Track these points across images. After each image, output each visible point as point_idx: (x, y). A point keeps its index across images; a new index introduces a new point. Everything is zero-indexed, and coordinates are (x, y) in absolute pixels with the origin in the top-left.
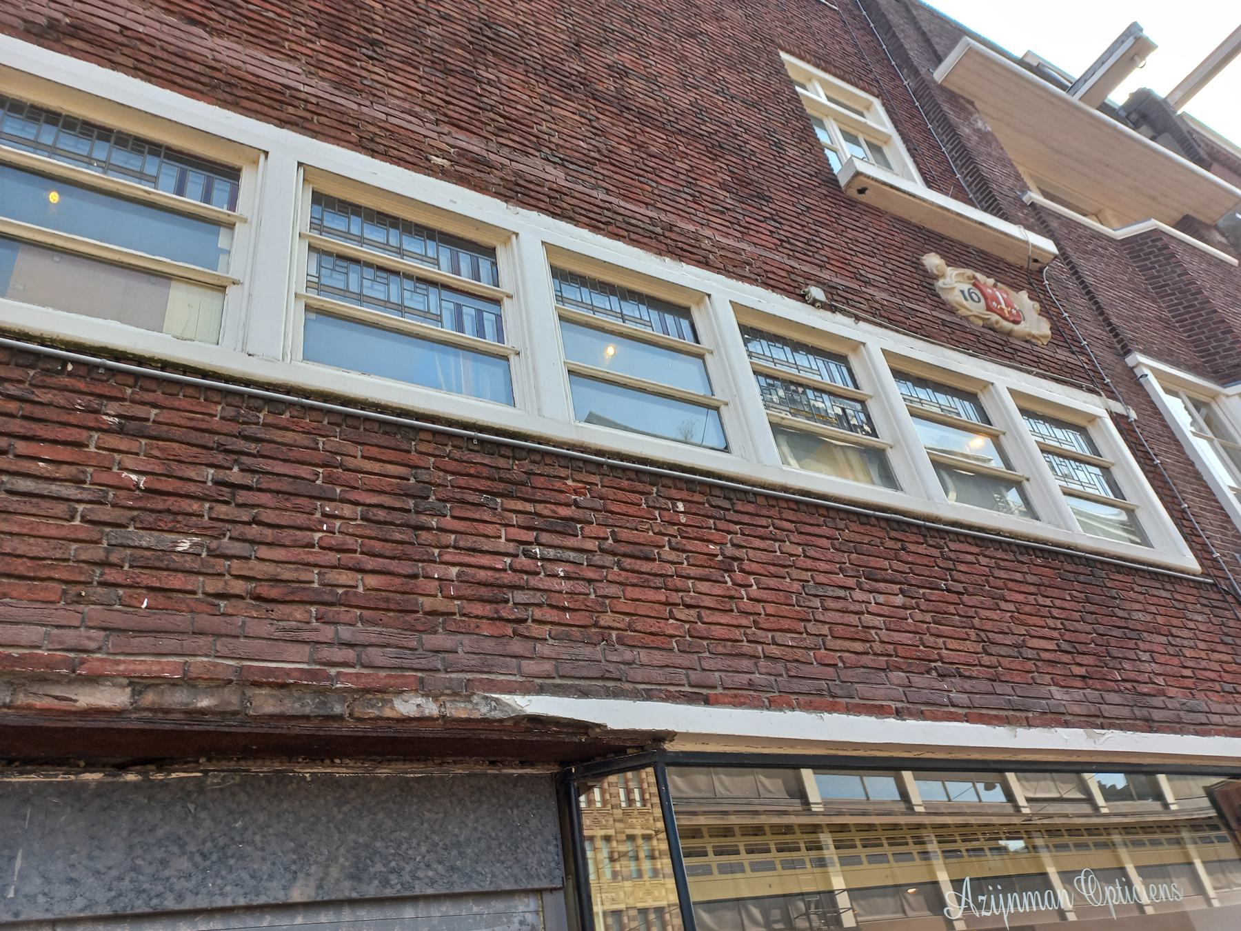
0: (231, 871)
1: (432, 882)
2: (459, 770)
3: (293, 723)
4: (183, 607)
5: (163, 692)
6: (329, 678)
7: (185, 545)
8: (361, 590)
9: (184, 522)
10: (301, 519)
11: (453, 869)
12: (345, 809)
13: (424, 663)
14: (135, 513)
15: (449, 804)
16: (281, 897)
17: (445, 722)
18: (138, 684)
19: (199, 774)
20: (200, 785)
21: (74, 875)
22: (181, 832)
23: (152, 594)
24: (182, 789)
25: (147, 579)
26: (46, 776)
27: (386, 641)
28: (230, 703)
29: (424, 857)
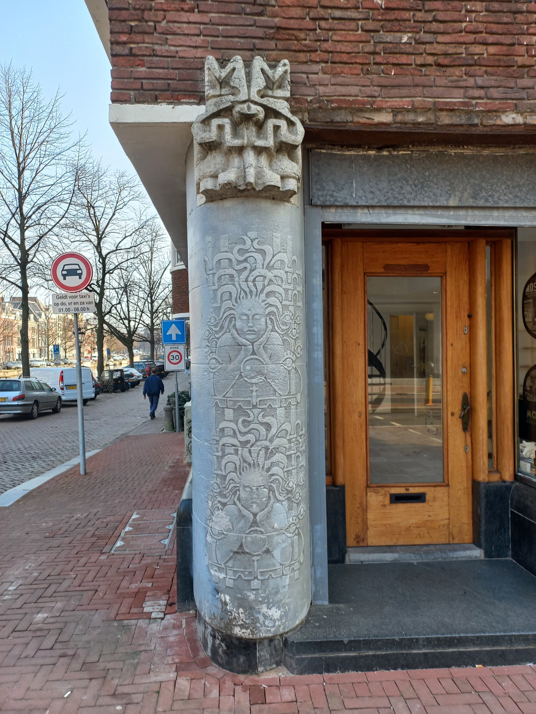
0: (426, 192)
1: (507, 202)
2: (521, 152)
3: (456, 128)
4: (408, 73)
5: (404, 115)
6: (472, 106)
7: (405, 39)
8: (485, 55)
9: (404, 25)
10: (455, 16)
11: (516, 196)
12: (469, 169)
13: (517, 95)
14: (382, 23)
15: (515, 168)
16: (445, 204)
17: (525, 127)
18: (395, 111)
19: (409, 152)
20: (410, 156)
21: (372, 190)
22: (406, 176)
23: (395, 67)
24: (404, 158)
25: (393, 59)
26: (357, 152)
27: (499, 84)
28: (430, 119)
29: (503, 191)
